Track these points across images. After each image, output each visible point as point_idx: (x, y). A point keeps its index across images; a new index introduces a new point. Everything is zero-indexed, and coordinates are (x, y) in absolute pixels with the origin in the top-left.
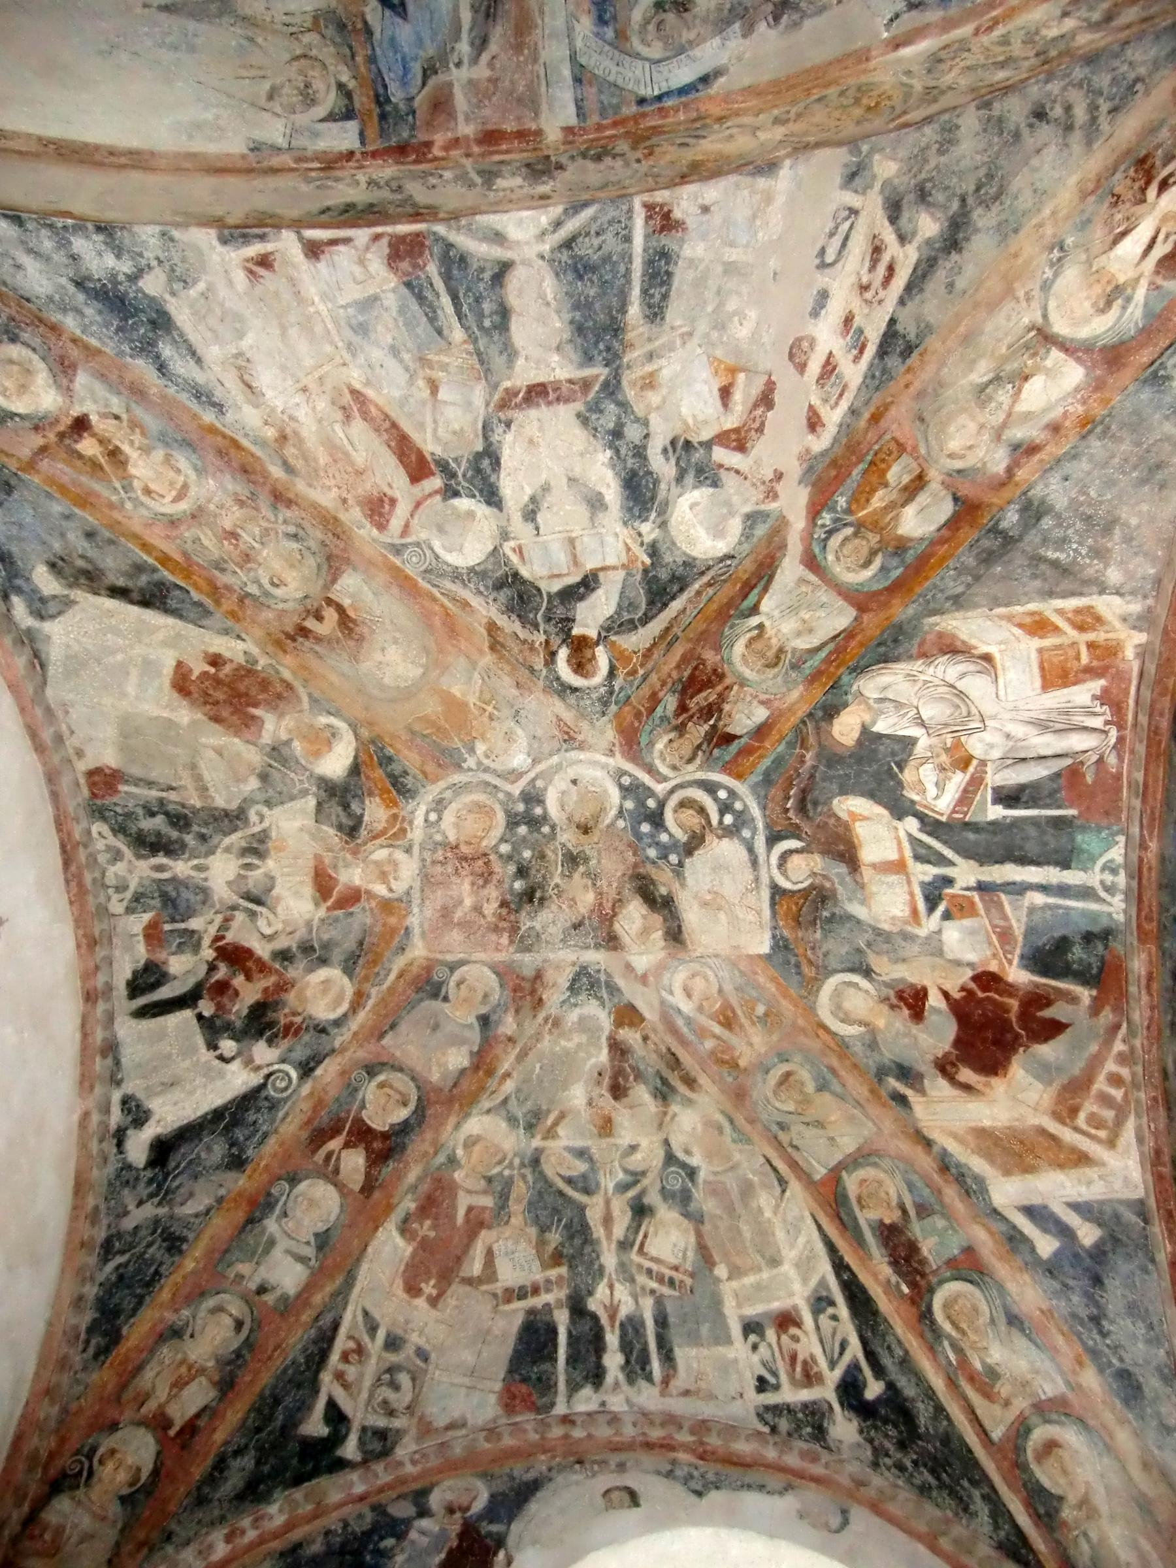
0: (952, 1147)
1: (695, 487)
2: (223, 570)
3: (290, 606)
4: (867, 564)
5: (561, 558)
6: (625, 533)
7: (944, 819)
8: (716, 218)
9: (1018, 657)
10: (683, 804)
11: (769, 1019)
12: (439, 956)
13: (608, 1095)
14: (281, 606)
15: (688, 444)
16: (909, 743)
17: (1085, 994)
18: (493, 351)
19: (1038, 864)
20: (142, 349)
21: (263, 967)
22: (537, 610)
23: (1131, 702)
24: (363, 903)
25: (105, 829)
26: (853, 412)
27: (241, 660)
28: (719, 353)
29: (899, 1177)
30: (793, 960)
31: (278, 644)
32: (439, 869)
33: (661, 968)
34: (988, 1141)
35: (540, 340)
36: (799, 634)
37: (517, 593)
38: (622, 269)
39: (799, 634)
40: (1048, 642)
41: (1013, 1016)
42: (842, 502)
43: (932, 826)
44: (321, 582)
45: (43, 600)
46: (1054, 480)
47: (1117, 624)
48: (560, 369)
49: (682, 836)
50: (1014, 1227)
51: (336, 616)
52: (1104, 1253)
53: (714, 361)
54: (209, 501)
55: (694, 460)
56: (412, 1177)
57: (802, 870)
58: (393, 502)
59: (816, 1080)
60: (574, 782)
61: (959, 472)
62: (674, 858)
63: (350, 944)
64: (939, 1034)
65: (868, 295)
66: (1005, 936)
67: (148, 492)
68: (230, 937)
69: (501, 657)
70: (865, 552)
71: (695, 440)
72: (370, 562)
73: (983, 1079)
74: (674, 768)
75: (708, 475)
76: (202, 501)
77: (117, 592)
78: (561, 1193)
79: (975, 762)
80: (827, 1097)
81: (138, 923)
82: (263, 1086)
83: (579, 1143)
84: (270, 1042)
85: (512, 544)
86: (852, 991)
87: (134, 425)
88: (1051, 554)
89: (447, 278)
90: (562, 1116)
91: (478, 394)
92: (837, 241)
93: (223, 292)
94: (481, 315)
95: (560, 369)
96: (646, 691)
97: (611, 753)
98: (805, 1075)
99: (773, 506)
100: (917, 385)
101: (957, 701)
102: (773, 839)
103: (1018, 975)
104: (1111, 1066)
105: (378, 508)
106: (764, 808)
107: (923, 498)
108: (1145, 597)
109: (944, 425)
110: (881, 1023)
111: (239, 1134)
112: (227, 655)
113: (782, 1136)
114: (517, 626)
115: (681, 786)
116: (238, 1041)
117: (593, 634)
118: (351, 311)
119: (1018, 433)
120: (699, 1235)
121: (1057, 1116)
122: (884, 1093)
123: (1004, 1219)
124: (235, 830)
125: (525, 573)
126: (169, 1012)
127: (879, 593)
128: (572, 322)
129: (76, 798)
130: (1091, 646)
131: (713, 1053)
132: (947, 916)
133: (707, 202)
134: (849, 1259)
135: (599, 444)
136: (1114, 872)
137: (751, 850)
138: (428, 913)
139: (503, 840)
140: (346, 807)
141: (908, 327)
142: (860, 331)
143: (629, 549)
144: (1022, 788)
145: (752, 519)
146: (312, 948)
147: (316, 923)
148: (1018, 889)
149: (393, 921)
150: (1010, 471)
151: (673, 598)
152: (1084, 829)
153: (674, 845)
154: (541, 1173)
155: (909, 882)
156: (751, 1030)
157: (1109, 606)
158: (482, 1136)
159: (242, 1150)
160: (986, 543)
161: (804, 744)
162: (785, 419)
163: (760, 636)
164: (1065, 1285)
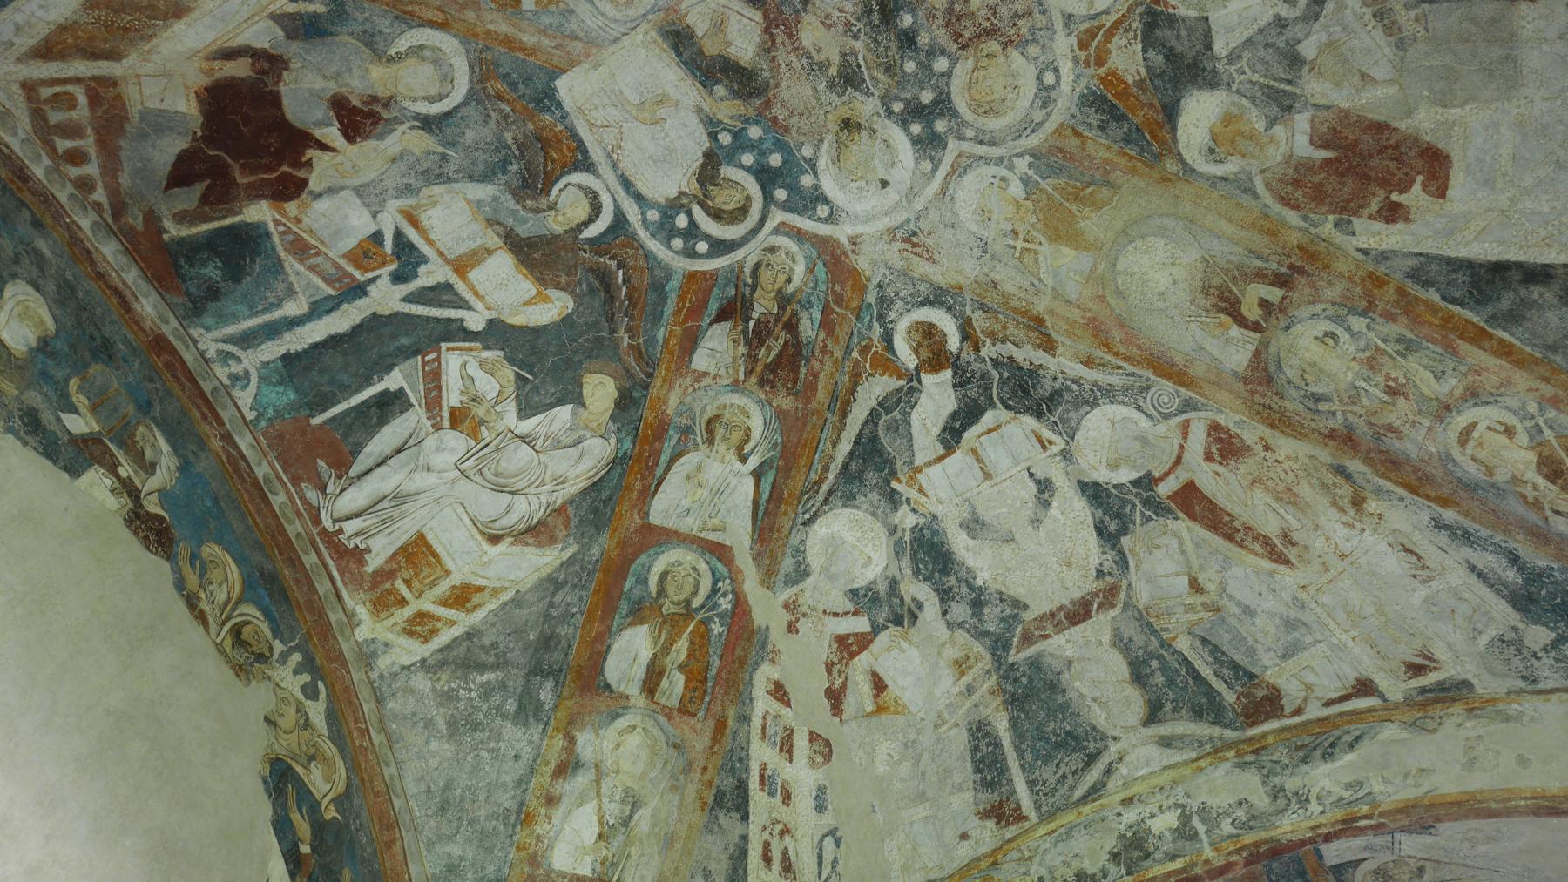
1: (874, 582)
2: (1400, 340)
3: (1304, 312)
4: (664, 576)
5: (993, 452)
6: (933, 507)
7: (444, 345)
8: (950, 835)
9: (463, 555)
14: (1319, 308)
15: (898, 621)
17: (174, 230)
18: (1139, 640)
19: (315, 346)
20: (1540, 575)
22: (1002, 383)
23: (330, 562)
26: (745, 718)
27: (1358, 223)
28: (900, 720)
30: (522, 89)
31: (1312, 256)
35: (1094, 670)
36: (699, 468)
37: (1028, 393)
38: (1028, 757)
39: (699, 468)
40: (443, 587)
42: (717, 628)
43: (455, 332)
44: (1272, 350)
46: (527, 753)
47: (391, 637)
48: (1061, 645)
49: (727, 171)
51: (1245, 311)
53: (899, 708)
54: (1430, 429)
55: (885, 608)
57: (567, 204)
58: (1209, 457)
60: (884, 184)
61: (618, 716)
62: (725, 139)
64: (303, 95)
65: (778, 827)
66: (301, 249)
67: (1509, 432)
69: (1025, 313)
70: (671, 590)
71: (892, 629)
72: (1218, 385)
73: (218, 75)
74: (772, 250)
75: (863, 599)
76: (1439, 429)
77: (1538, 275)
79: (446, 423)
85: (1055, 449)
86: (433, 92)
87: (1537, 505)
88: (490, 676)
89: (1211, 693)
91: (1143, 596)
92: (828, 857)
93: (1458, 638)
94: (1164, 668)
95: (1061, 645)
96: (842, 334)
99: (786, 594)
100: (696, 776)
101: (501, 481)
102: (620, 219)
104: (92, 169)
105: (1225, 447)
106: (648, 255)
107: (639, 672)
108: (381, 677)
109: (654, 752)
110: (377, 72)
112: (1378, 226)
114: (1019, 355)
115: (755, 231)
117: (928, 379)
118: (1308, 639)
119: (581, 780)
121: (111, 82)
125: (1029, 422)
127: (637, 555)
128: (1064, 691)
130: (403, 602)
132: (377, 237)
133: (966, 843)
135: (993, 587)
136: (234, 378)
137: (639, 198)
139: (948, 75)
140: (1171, 55)
141: (728, 821)
142: (771, 794)
143: (921, 491)
144: (383, 422)
145: (801, 573)
148: (319, 309)
150: (572, 740)
151: (851, 454)
152: (292, 407)
153: (732, 154)
155: (441, 254)
157: (409, 651)
160: (557, 656)
161: (638, 352)
162: (810, 686)
163: (740, 448)
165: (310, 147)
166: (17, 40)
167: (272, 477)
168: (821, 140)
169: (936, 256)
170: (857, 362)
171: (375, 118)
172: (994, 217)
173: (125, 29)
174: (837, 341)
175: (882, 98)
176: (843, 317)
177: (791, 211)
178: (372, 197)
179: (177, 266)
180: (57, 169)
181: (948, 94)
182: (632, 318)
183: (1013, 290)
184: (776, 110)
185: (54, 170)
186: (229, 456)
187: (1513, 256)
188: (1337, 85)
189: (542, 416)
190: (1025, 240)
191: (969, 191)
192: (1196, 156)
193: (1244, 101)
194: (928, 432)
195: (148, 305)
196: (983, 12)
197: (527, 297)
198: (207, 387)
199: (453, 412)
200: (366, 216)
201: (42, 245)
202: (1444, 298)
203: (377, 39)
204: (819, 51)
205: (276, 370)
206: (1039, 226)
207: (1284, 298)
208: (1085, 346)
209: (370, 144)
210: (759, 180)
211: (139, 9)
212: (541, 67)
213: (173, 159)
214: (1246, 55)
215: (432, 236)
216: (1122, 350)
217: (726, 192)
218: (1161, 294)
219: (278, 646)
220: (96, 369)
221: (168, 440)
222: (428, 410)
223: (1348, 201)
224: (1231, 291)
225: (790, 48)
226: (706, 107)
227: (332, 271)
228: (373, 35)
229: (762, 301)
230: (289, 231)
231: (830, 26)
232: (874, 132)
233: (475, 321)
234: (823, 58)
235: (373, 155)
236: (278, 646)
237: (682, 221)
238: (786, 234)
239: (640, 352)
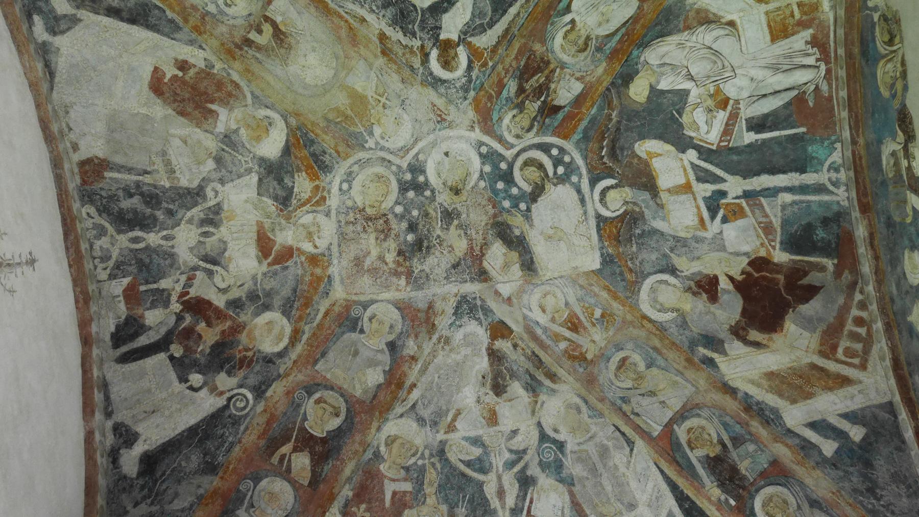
0: (752, 390)
3: (239, 22)
7: (714, 148)
10: (526, 164)
11: (606, 318)
12: (355, 298)
13: (491, 393)
14: (231, 22)
16: (684, 94)
17: (829, 263)
19: (784, 172)
21: (220, 314)
22: (414, 22)
23: (832, 44)
24: (295, 258)
25: (92, 210)
27: (202, 65)
29: (716, 420)
30: (618, 271)
31: (229, 52)
32: (351, 228)
33: (521, 292)
34: (777, 381)
36: (600, 24)
39: (600, 24)
41: (781, 286)
43: (706, 153)
45: (57, 19)
49: (528, 188)
50: (805, 440)
51: (271, 30)
52: (870, 444)
56: (347, 471)
57: (618, 201)
59: (645, 360)
60: (447, 154)
62: (523, 206)
63: (286, 292)
64: (730, 309)
66: (768, 229)
68: (193, 292)
69: (390, 60)
73: (766, 336)
74: (518, 137)
78: (464, 475)
79: (731, 102)
80: (654, 371)
81: (118, 287)
82: (227, 407)
83: (473, 434)
84: (229, 373)
86: (663, 286)
90: (458, 413)
96: (495, 78)
97: (472, 128)
98: (636, 358)
101: (713, 58)
102: (593, 183)
103: (781, 257)
104: (855, 312)
106: (585, 158)
110: (687, 307)
111: (210, 445)
112: (192, 61)
113: (625, 408)
114: (399, 36)
116: (204, 374)
117: (455, 37)
120: (572, 495)
121: (822, 354)
122: (696, 360)
123: (798, 436)
124: (196, 204)
126: (147, 356)
129: (73, 183)
131: (566, 351)
134: (689, 492)
136: (837, 170)
137: (579, 191)
138: (344, 263)
139: (397, 203)
140: (280, 181)
144: (766, 116)
146: (258, 297)
147: (259, 277)
148: (773, 192)
149: (318, 271)
152: (813, 142)
153: (522, 196)
154: (447, 460)
155: (695, 199)
156: (592, 330)
158: (399, 433)
159: (214, 457)
161: (610, 106)
163: (572, 29)
164: (846, 472)
165: (739, 282)
166: (856, 392)
167: (841, 108)
168: (473, 188)
169: (430, 106)
170: (491, 59)
171: (699, 284)
172: (393, 119)
173: (801, 377)
174: (498, 74)
175: (435, 200)
176: (491, 87)
177: (501, 155)
178: (719, 244)
179: (837, 245)
180: (872, 321)
181: (399, 192)
182: (606, 126)
183: (394, 75)
184: (491, 211)
185: (873, 321)
186: (857, 132)
187: (124, 26)
188: (199, 142)
189: (676, 88)
190: (379, 101)
191: (402, 137)
192: (279, 123)
193: (248, 147)
194: (463, 5)
195: (861, 232)
196: (370, 230)
197: (658, 159)
198: (852, 173)
199: (724, 109)
200: (725, 234)
201: (895, 291)
202: (164, 11)
203: (680, 323)
204: (459, 236)
205: (812, 167)
206: (370, 107)
207: (249, 32)
208: (362, 31)
209: (706, 272)
210: (513, 178)
211: (789, 384)
212: (604, 278)
213: (811, 302)
214: (242, 170)
215: (696, 210)
216: (342, 23)
217: (532, 178)
218: (314, 51)
219: (876, 17)
220: (897, 219)
221: (881, 160)
222: (738, 114)
223: (205, 78)
224: (276, 43)
225: (474, 242)
226: (527, 226)
227: (757, 211)
228: (681, 326)
229: (532, 109)
230: (770, 241)
231: (450, 246)
232: (444, 184)
233: (692, 155)
234: (459, 231)
235: (708, 265)
236: (876, 17)
237: (561, 170)
238: (508, 143)
239: (609, 105)
